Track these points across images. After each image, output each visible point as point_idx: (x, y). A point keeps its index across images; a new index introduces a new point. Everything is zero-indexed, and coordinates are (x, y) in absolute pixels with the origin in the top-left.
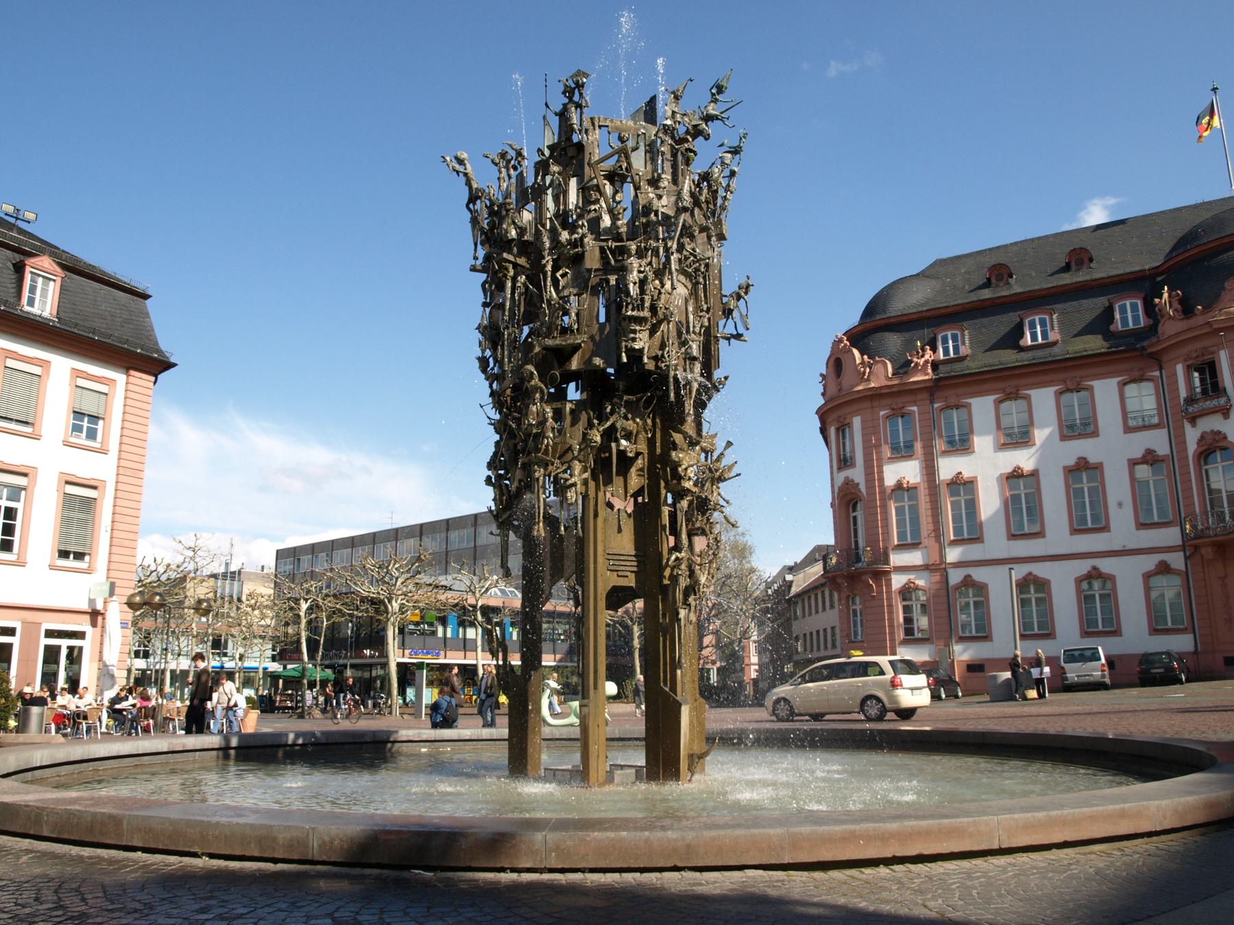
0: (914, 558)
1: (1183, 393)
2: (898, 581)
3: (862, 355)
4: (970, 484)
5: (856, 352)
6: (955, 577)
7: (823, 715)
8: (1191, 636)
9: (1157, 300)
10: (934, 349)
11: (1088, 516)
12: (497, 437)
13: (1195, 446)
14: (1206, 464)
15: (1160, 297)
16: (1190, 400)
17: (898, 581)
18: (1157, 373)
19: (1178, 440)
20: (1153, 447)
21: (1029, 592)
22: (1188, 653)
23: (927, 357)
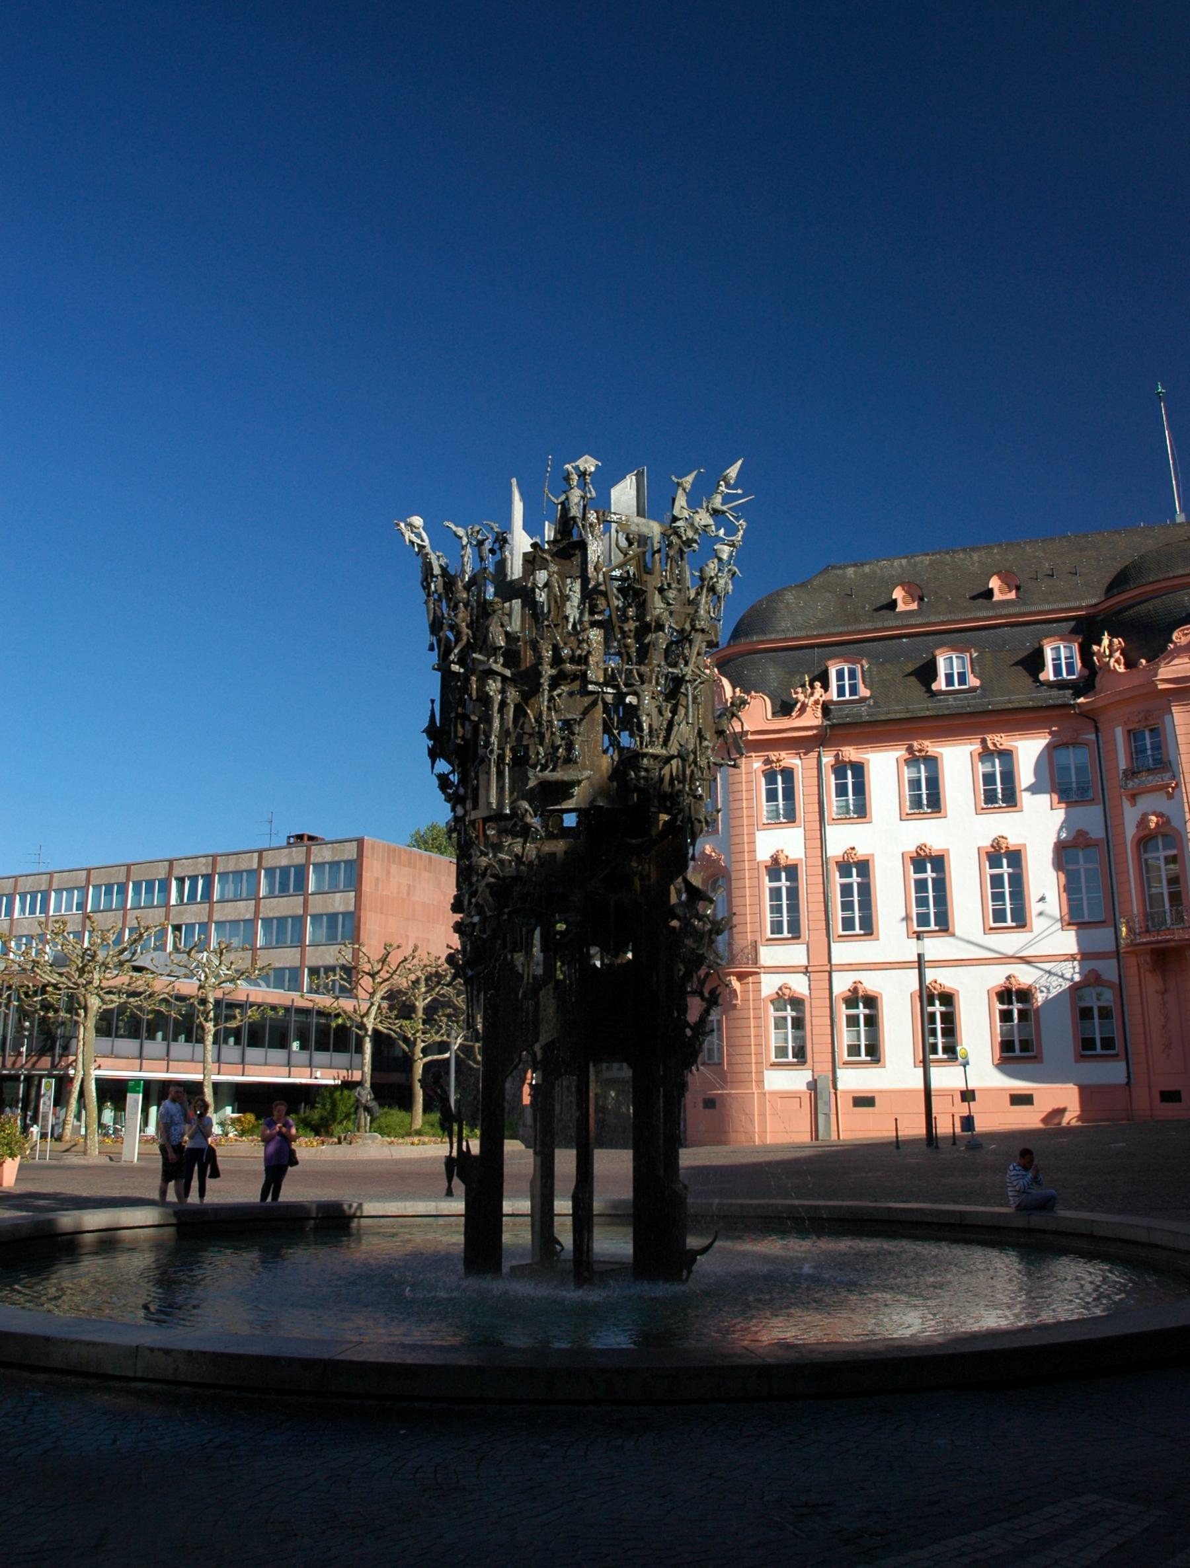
0: (796, 954)
1: (1123, 764)
2: (769, 985)
3: (734, 688)
4: (864, 867)
5: (725, 682)
6: (842, 984)
7: (85, 1108)
8: (1123, 1064)
9: (1095, 648)
10: (826, 687)
11: (1009, 904)
12: (456, 941)
13: (1135, 830)
14: (1145, 852)
15: (1099, 643)
16: (1131, 773)
17: (769, 985)
18: (1093, 737)
19: (1111, 822)
20: (1086, 829)
21: (1077, 862)
22: (1119, 1086)
23: (816, 696)
